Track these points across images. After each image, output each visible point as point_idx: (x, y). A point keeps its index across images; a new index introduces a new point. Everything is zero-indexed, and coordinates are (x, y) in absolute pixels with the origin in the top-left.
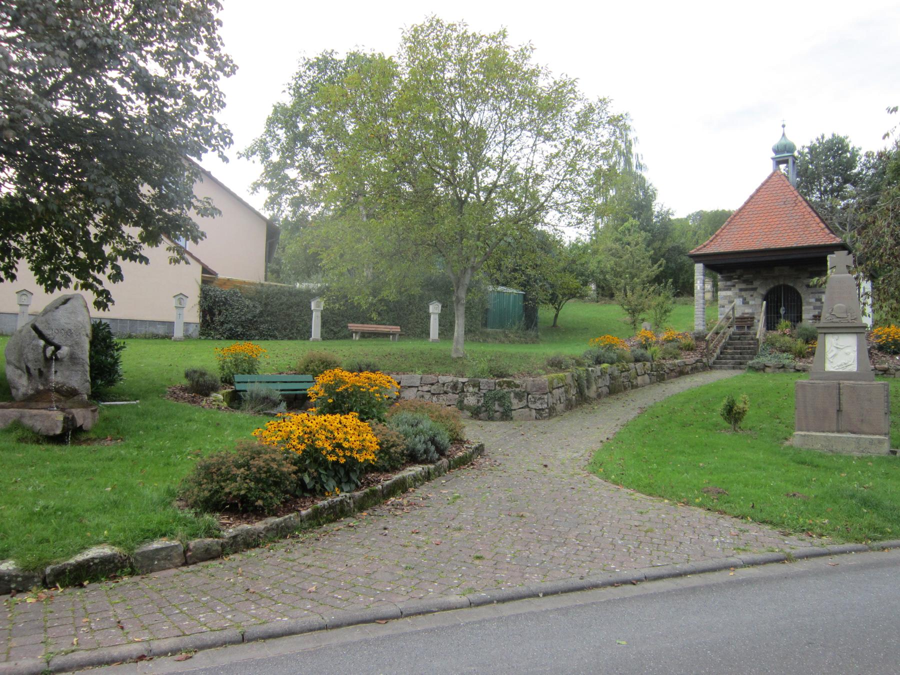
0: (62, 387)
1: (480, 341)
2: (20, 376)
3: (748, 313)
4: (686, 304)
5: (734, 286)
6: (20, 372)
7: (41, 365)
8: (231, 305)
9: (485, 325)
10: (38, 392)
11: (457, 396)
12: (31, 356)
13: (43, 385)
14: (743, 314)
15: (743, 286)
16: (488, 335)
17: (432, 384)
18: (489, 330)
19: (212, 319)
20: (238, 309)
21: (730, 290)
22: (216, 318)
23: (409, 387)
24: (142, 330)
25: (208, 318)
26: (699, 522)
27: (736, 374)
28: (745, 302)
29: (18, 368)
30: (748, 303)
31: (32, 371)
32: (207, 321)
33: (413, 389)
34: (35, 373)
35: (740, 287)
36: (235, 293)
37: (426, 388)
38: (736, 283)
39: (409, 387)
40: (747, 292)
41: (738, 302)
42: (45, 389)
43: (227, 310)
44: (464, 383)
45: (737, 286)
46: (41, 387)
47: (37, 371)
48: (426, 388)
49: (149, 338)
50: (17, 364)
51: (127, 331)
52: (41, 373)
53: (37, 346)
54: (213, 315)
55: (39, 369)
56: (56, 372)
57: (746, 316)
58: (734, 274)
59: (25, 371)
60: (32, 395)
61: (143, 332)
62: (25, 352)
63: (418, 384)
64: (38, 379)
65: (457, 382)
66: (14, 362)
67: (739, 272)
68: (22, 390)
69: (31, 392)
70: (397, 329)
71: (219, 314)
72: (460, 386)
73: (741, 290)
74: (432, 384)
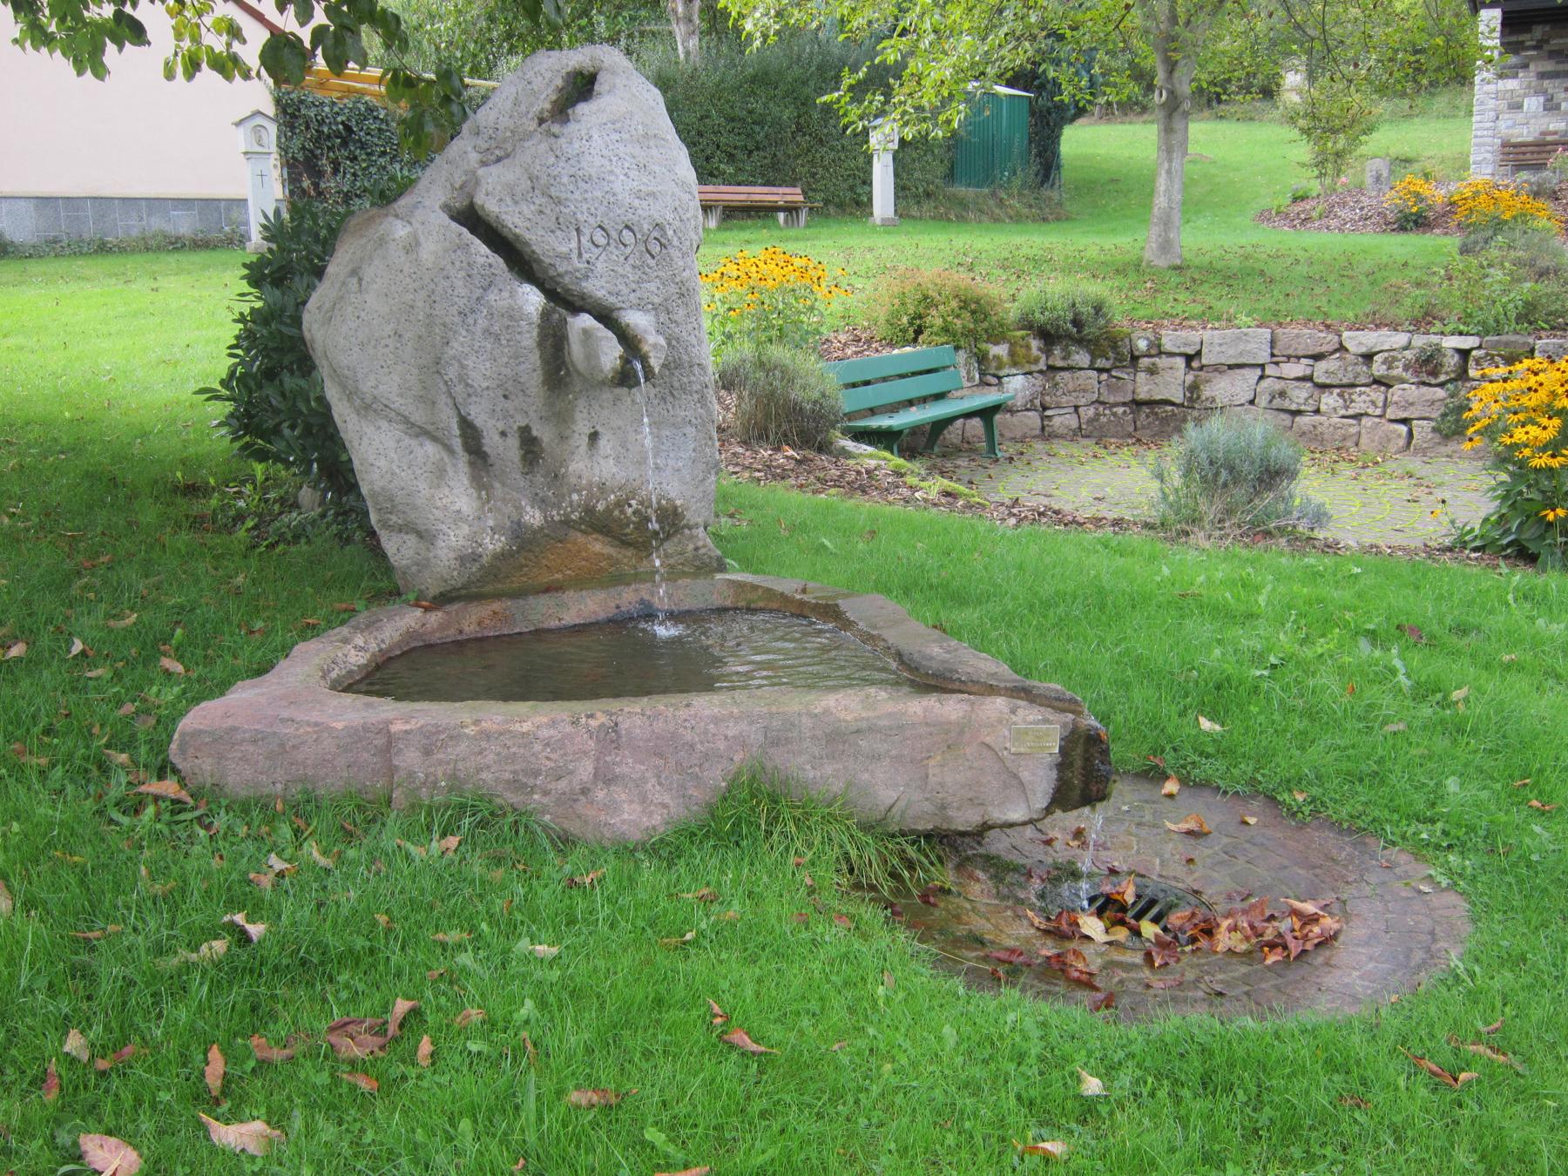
0: (619, 504)
1: (949, 220)
2: (440, 474)
3: (1555, 133)
4: (1251, 119)
5: (1525, 66)
6: (431, 449)
7: (531, 408)
8: (363, 146)
9: (951, 176)
10: (524, 542)
11: (1440, 393)
12: (481, 371)
13: (541, 503)
14: (1543, 133)
15: (1549, 66)
16: (963, 204)
17: (1318, 357)
18: (961, 190)
19: (316, 185)
20: (384, 153)
21: (1515, 76)
22: (330, 184)
23: (1231, 367)
24: (131, 226)
25: (306, 183)
26: (1441, 597)
27: (491, 260)
28: (1551, 106)
29: (422, 432)
30: (1558, 107)
31: (491, 441)
32: (304, 191)
33: (1245, 371)
34: (504, 450)
35: (1541, 69)
36: (370, 109)
37: (1298, 369)
38: (1531, 58)
39: (1231, 367)
40: (1557, 82)
41: (1533, 104)
42: (550, 522)
43: (354, 159)
44: (1464, 354)
45: (1532, 67)
46: (534, 517)
47: (514, 442)
48: (1298, 369)
49: (159, 249)
50: (418, 417)
51: (90, 231)
52: (530, 446)
53: (513, 315)
54: (317, 174)
55: (525, 432)
56: (594, 437)
57: (1549, 138)
58: (1528, 36)
59: (457, 443)
60: (502, 556)
61: (135, 233)
62: (456, 348)
63: (1264, 357)
64: (517, 477)
65: (1438, 350)
66: (398, 403)
67: (1538, 32)
68: (452, 541)
69: (493, 544)
70: (794, 195)
71: (336, 171)
72: (1452, 361)
73: (1542, 76)
74: (1318, 357)
